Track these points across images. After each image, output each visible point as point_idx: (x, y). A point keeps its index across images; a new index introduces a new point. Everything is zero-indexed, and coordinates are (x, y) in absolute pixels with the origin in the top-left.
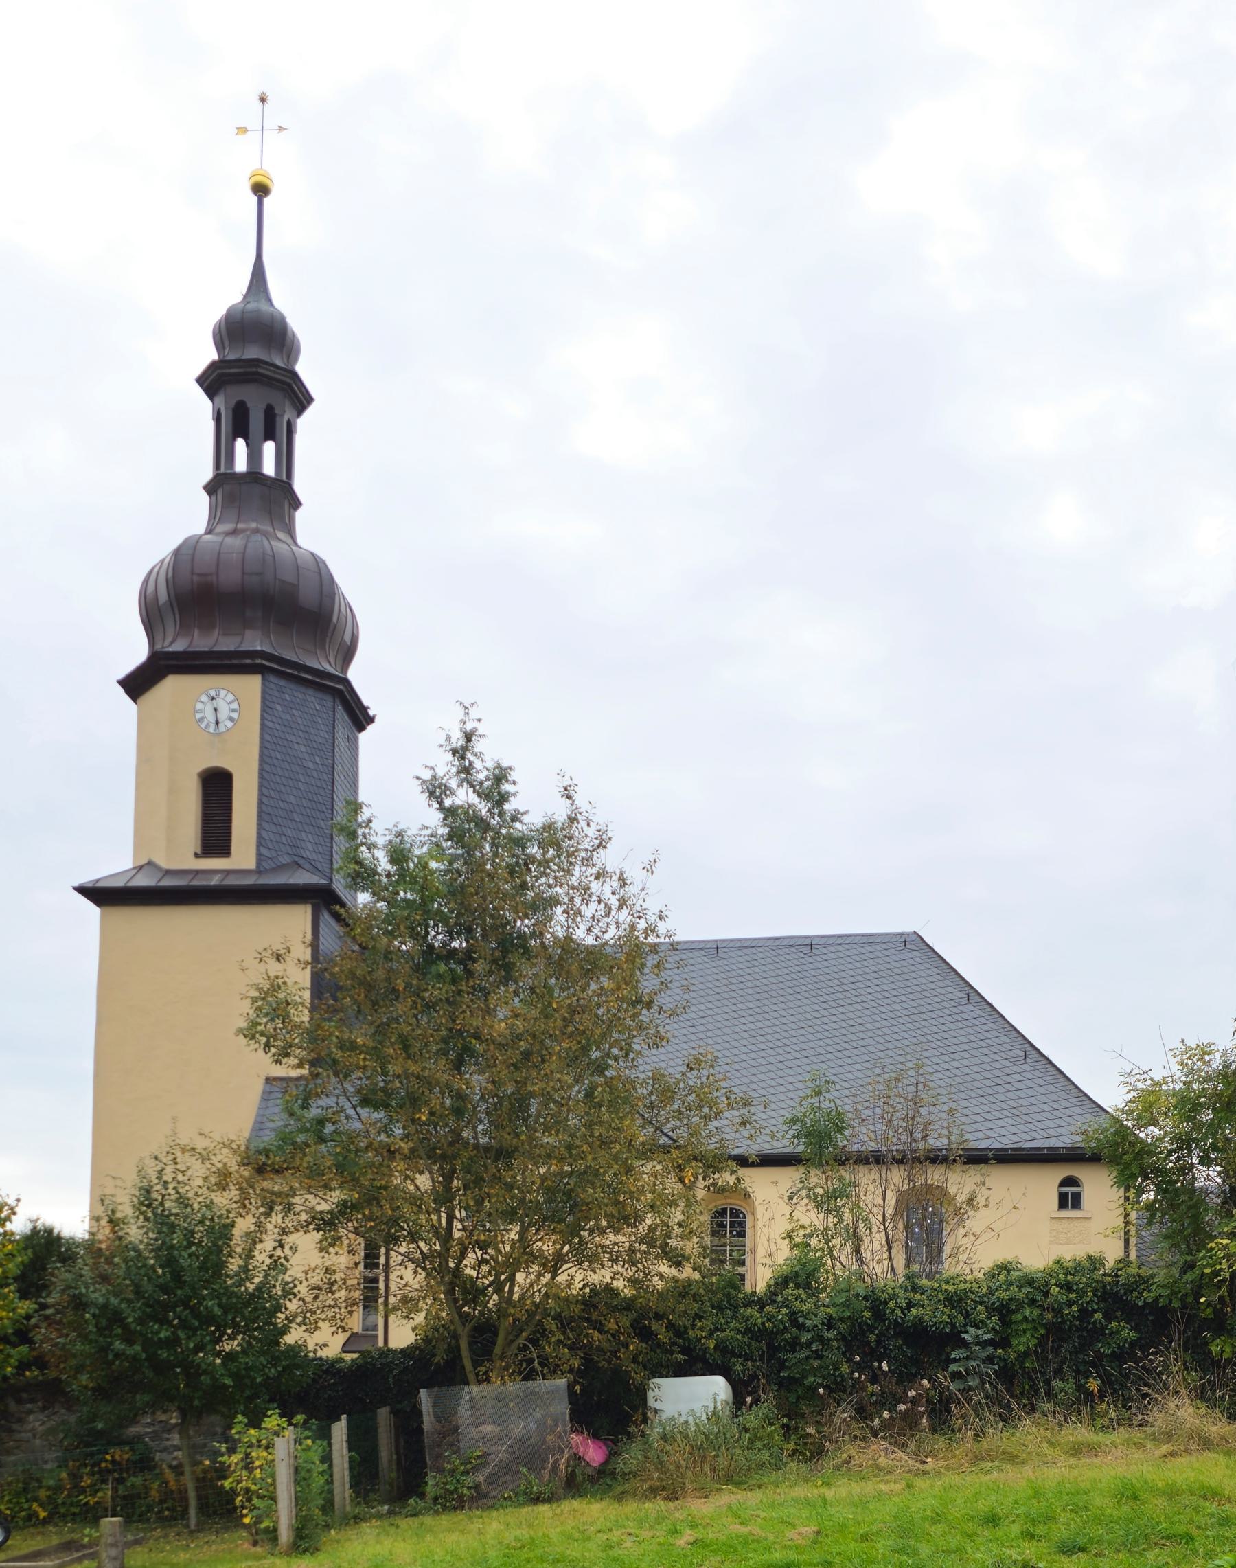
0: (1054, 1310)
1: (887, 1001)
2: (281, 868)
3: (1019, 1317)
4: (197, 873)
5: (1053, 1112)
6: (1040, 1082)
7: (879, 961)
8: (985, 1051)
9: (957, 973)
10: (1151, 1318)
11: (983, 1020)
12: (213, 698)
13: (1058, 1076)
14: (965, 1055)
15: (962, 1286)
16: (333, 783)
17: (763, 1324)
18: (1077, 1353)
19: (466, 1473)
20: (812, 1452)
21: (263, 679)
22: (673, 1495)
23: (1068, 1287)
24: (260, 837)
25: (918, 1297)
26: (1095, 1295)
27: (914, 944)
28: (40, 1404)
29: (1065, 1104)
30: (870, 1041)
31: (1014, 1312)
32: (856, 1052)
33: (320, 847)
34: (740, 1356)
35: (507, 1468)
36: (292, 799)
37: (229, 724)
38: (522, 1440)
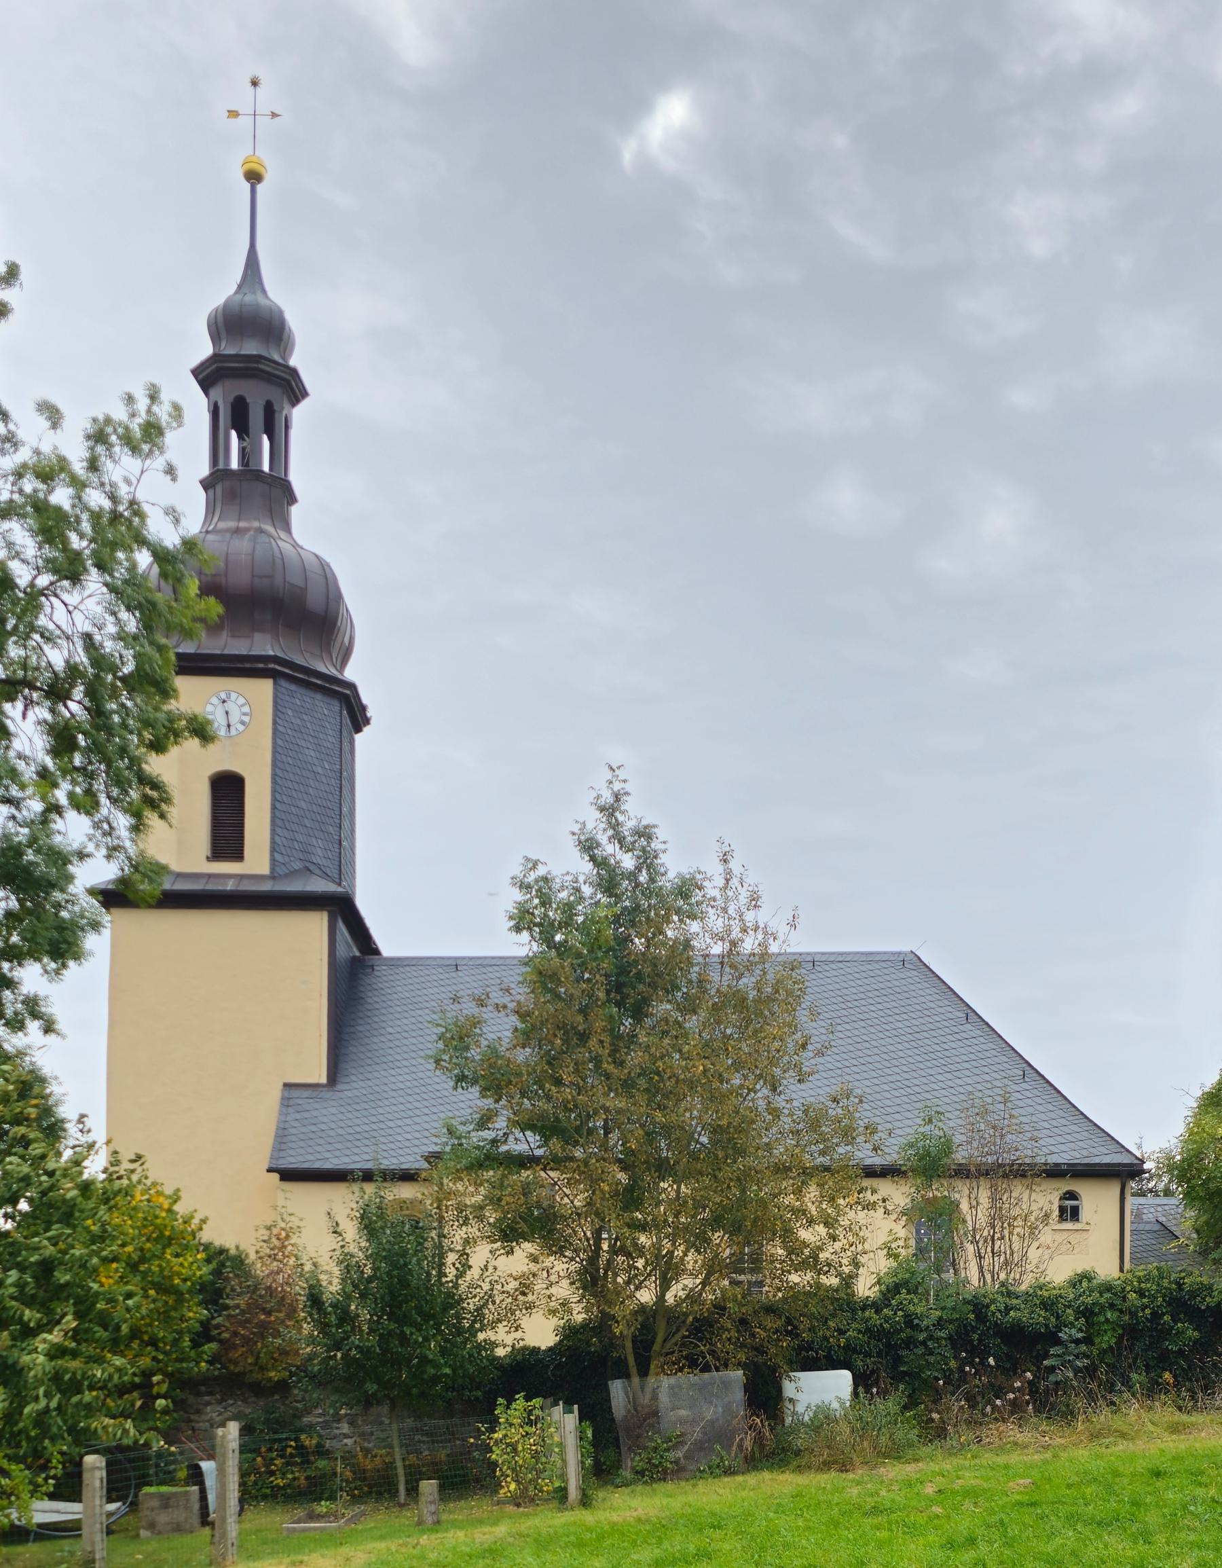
0: (1130, 1313)
1: (890, 1019)
2: (293, 874)
3: (1102, 1319)
4: (210, 876)
5: (1054, 1130)
6: (1039, 1100)
7: (880, 979)
8: (986, 1070)
9: (955, 993)
10: (1211, 1320)
11: (982, 1040)
12: (224, 702)
13: (1056, 1095)
14: (967, 1073)
15: (1055, 1292)
16: (341, 788)
17: (881, 1324)
18: (1146, 1350)
19: (667, 1450)
20: (937, 1433)
21: (275, 683)
22: (844, 1468)
23: (1141, 1293)
24: (273, 843)
25: (1015, 1301)
26: (1164, 1300)
27: (913, 963)
28: (218, 1396)
29: (1064, 1122)
30: (877, 1058)
31: (1096, 1314)
32: (864, 1068)
33: (329, 852)
34: (860, 1353)
35: (701, 1447)
36: (303, 805)
37: (241, 728)
38: (712, 1422)
